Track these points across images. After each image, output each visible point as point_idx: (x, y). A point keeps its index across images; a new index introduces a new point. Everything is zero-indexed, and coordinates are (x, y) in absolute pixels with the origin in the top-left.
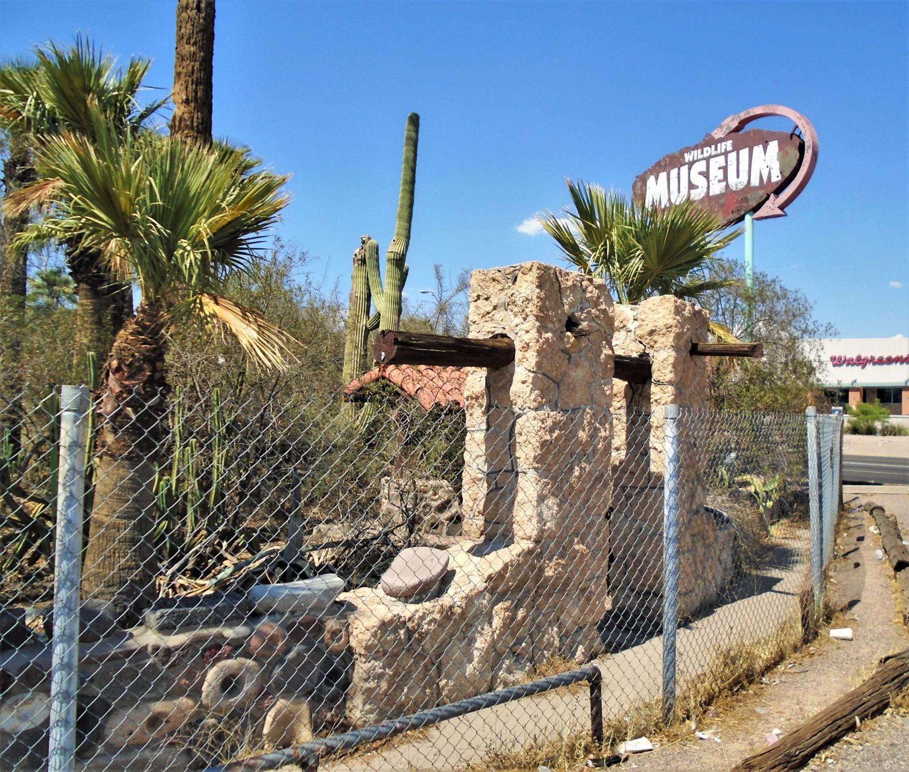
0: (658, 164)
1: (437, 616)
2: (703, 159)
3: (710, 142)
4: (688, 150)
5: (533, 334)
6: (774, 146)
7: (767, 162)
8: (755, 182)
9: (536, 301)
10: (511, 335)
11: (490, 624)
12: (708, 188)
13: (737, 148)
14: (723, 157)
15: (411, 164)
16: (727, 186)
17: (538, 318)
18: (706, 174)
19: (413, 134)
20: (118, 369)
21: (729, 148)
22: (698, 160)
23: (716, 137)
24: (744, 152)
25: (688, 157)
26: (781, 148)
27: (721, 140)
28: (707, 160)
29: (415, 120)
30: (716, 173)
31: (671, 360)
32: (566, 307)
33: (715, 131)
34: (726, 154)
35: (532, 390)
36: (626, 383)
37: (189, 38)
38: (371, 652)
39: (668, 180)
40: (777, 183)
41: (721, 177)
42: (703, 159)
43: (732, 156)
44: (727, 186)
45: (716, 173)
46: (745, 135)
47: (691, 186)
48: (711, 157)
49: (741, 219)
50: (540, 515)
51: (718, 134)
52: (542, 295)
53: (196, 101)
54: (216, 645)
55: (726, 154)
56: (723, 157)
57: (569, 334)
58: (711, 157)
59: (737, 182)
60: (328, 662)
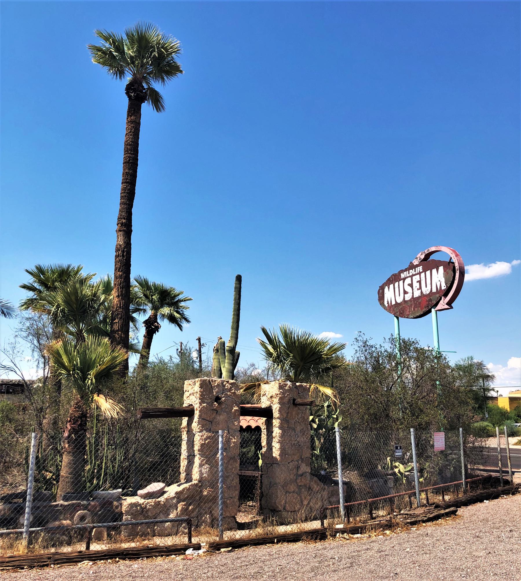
0: (389, 279)
1: (153, 504)
2: (409, 277)
3: (412, 267)
4: (402, 271)
5: (198, 405)
6: (441, 269)
7: (438, 278)
8: (434, 290)
9: (199, 392)
10: (194, 405)
11: (177, 509)
12: (413, 293)
13: (425, 271)
14: (418, 275)
15: (238, 301)
16: (422, 292)
17: (200, 399)
18: (411, 285)
19: (238, 286)
20: (70, 421)
21: (421, 271)
22: (407, 277)
23: (415, 264)
24: (428, 273)
25: (403, 276)
26: (445, 271)
27: (417, 266)
28: (411, 277)
29: (239, 279)
30: (416, 285)
31: (278, 408)
32: (215, 393)
33: (414, 261)
34: (420, 273)
35: (198, 425)
36: (265, 419)
37: (119, 269)
38: (127, 513)
39: (394, 288)
40: (444, 290)
41: (418, 287)
42: (409, 277)
43: (423, 275)
44: (422, 292)
45: (416, 285)
46: (428, 263)
47: (405, 292)
48: (413, 275)
49: (429, 311)
50: (201, 471)
51: (416, 262)
52: (202, 390)
53: (122, 296)
54: (79, 505)
55: (420, 273)
56: (418, 275)
57: (215, 403)
58: (413, 275)
59: (426, 291)
60: (115, 515)
